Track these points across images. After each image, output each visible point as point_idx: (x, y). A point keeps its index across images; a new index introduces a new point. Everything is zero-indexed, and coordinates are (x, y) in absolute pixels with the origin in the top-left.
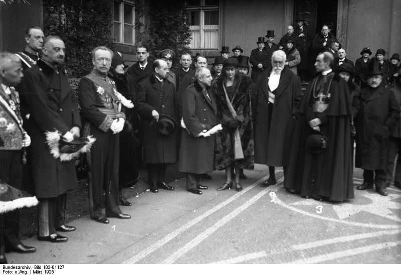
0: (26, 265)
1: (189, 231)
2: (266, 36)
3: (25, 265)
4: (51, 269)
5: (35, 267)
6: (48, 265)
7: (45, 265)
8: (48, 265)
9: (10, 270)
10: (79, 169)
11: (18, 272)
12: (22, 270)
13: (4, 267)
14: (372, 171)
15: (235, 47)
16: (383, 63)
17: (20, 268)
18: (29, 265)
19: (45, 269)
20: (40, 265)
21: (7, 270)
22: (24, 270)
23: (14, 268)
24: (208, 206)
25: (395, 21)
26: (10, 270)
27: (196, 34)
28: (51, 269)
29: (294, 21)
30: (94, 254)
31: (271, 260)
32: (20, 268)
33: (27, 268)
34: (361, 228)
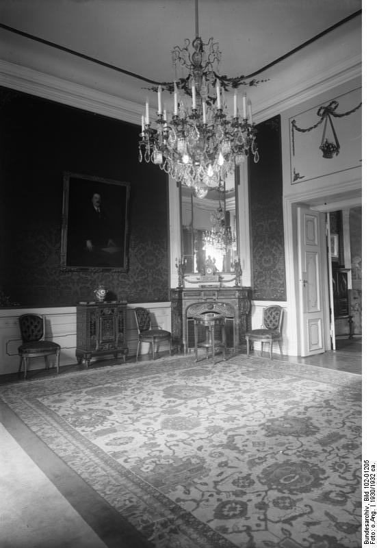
0: (363, 512)
1: (250, 347)
2: (250, 475)
4: (369, 478)
5: (366, 500)
7: (363, 486)
8: (363, 483)
9: (370, 535)
10: (110, 250)
11: (373, 523)
12: (370, 517)
13: (366, 543)
14: (336, 349)
15: (320, 150)
16: (98, 289)
17: (367, 521)
19: (369, 486)
20: (363, 494)
21: (370, 538)
22: (370, 515)
23: (367, 529)
26: (370, 535)
28: (369, 478)
29: (182, 253)
32: (367, 521)
33: (368, 511)
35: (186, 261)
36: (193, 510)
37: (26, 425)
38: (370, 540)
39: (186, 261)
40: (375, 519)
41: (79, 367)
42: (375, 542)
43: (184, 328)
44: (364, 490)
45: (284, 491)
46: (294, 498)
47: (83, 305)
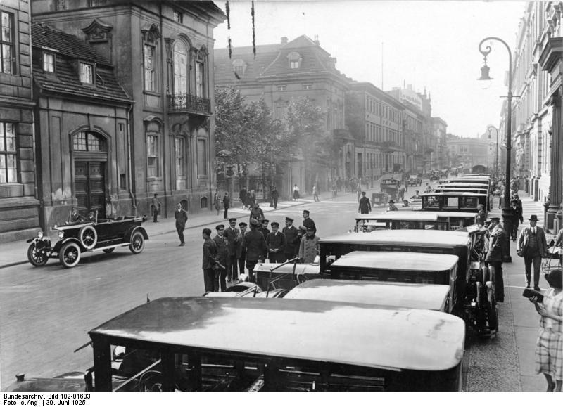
0: (37, 393)
5: (50, 396)
7: (64, 393)
8: (67, 393)
9: (14, 400)
11: (26, 403)
12: (31, 400)
13: (5, 396)
17: (27, 397)
18: (41, 393)
20: (55, 393)
21: (10, 400)
22: (34, 400)
23: (20, 397)
26: (14, 400)
32: (27, 397)
33: (38, 397)
35: (49, 64)
36: (174, 231)
39: (49, 64)
41: (131, 112)
43: (146, 82)
44: (60, 393)
45: (293, 127)
46: (233, 186)
47: (328, 272)
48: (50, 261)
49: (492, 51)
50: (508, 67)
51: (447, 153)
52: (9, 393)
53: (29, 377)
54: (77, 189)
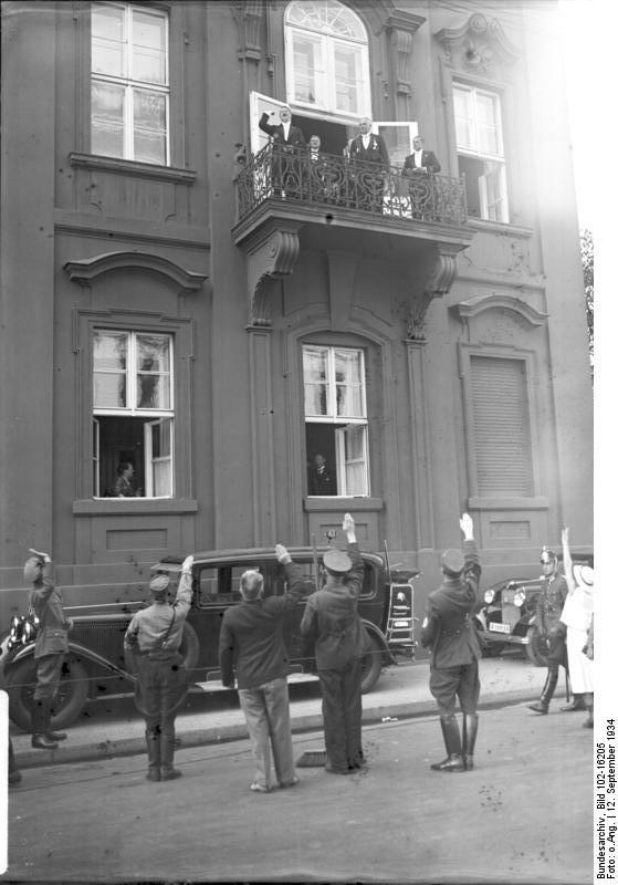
3: (595, 858)
5: (601, 807)
6: (596, 780)
9: (607, 864)
11: (611, 845)
12: (607, 836)
13: (601, 876)
17: (602, 842)
18: (596, 821)
21: (607, 869)
22: (607, 832)
23: (602, 854)
24: (352, 780)
25: (459, 4)
26: (607, 864)
27: (292, 247)
30: (320, 390)
31: (320, 54)
32: (602, 842)
33: (603, 826)
34: (515, 304)
37: (214, 567)
38: (607, 871)
40: (615, 839)
42: (615, 875)
48: (318, 845)
49: (67, 153)
50: (337, 330)
51: (134, 640)
52: (597, 870)
53: (270, 122)
54: (213, 549)
